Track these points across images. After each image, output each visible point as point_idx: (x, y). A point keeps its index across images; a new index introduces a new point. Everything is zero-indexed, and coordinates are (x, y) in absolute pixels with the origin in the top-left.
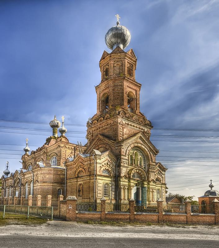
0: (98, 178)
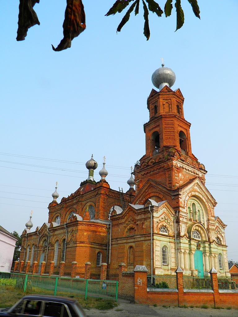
0: (155, 237)
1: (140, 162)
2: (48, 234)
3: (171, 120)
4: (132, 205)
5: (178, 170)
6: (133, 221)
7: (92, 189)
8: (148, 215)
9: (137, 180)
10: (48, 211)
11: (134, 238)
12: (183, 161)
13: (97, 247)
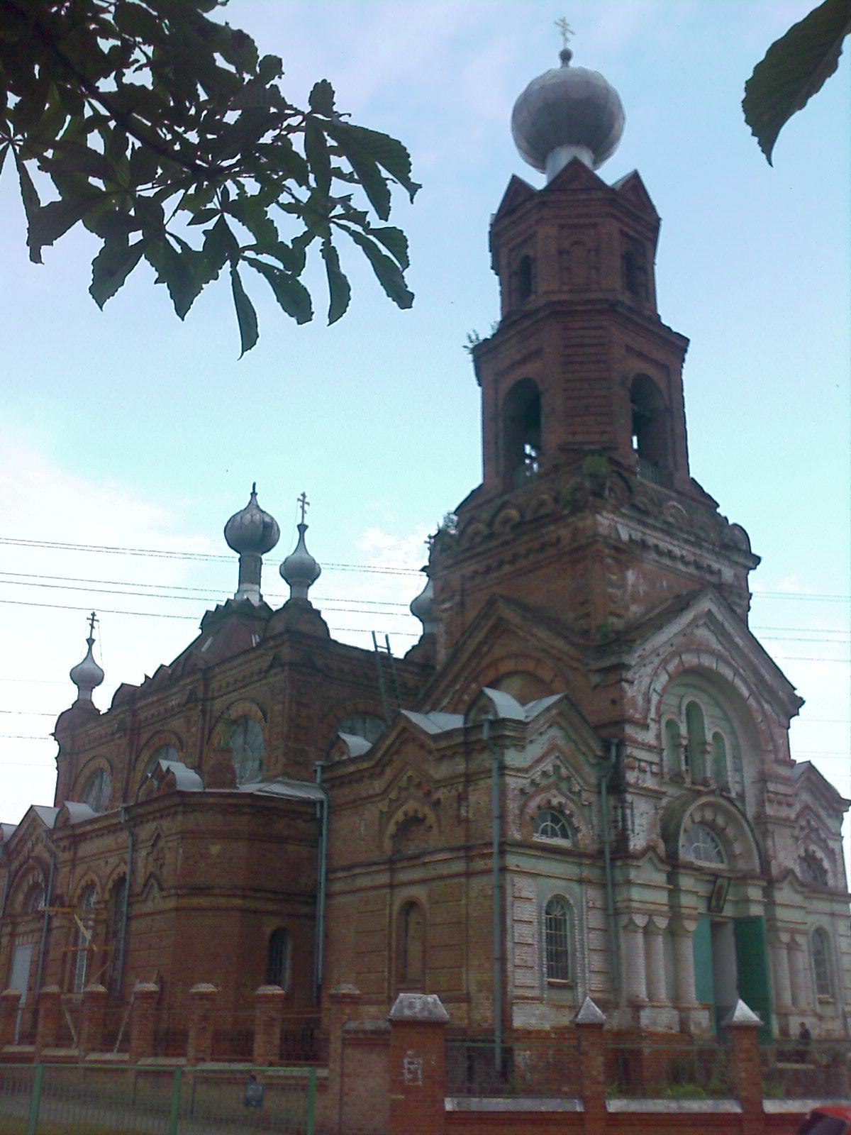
1: (455, 518)
2: (46, 856)
4: (415, 718)
5: (623, 557)
6: (419, 786)
7: (255, 640)
8: (486, 760)
9: (443, 602)
11: (424, 864)
12: (646, 513)
13: (271, 907)
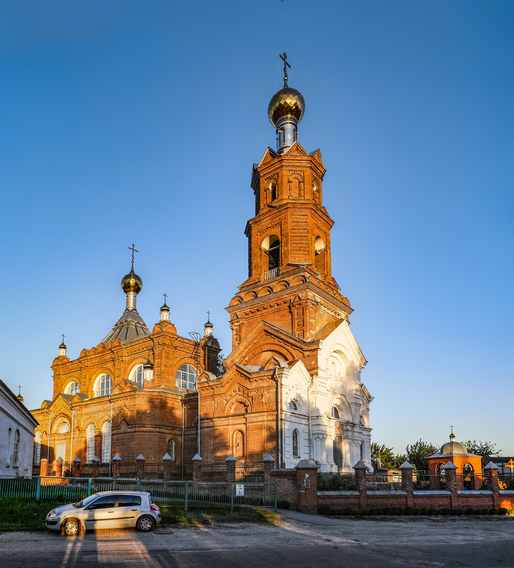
3: (303, 214)
10: (52, 373)
